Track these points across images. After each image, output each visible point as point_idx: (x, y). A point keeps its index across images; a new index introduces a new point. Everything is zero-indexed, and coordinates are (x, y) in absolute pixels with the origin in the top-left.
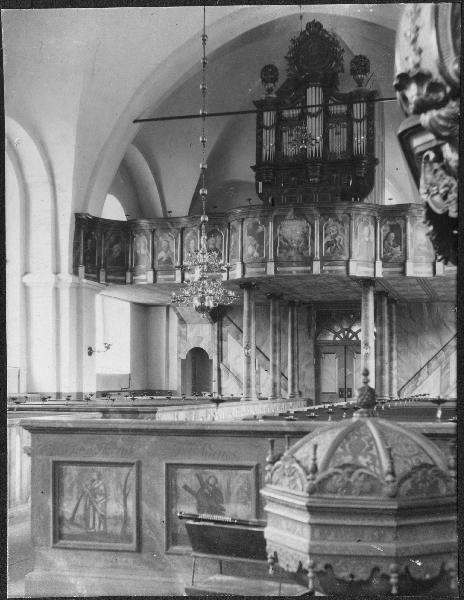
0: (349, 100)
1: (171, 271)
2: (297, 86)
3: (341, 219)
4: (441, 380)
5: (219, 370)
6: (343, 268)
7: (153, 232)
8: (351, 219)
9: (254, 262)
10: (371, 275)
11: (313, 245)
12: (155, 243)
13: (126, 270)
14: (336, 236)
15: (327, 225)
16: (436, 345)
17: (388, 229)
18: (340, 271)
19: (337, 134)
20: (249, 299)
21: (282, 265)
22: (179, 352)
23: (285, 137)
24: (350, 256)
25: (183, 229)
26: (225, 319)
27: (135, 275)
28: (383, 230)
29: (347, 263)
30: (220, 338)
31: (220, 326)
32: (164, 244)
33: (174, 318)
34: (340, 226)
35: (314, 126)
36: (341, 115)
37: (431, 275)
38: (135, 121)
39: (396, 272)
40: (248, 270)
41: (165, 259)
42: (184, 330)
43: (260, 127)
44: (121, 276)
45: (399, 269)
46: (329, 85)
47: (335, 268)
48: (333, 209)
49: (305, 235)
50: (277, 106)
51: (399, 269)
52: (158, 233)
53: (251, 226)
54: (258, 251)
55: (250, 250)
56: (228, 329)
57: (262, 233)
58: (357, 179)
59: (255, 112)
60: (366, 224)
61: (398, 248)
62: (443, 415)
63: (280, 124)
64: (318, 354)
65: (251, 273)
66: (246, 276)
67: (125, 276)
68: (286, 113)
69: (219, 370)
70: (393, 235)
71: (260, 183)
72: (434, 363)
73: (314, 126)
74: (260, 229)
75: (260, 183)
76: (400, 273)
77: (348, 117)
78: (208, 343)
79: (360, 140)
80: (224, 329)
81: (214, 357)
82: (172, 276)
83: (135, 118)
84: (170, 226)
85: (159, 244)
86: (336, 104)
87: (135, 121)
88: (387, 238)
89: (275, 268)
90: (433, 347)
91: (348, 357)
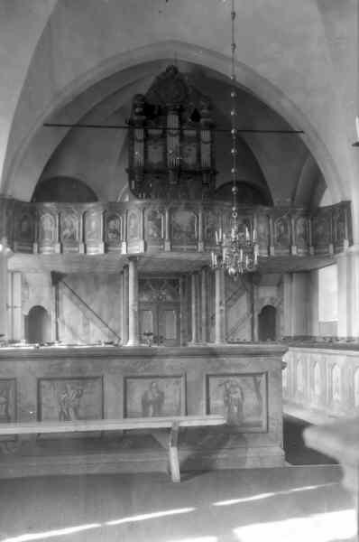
1: (76, 245)
5: (57, 323)
13: (33, 242)
18: (68, 247)
19: (155, 148)
21: (177, 244)
23: (151, 148)
25: (85, 213)
30: (57, 298)
31: (57, 289)
32: (69, 224)
33: (17, 278)
35: (173, 142)
38: (46, 125)
41: (69, 235)
42: (26, 292)
49: (192, 223)
50: (144, 125)
51: (110, 248)
57: (161, 220)
59: (125, 127)
63: (147, 138)
67: (32, 246)
68: (152, 132)
69: (57, 323)
73: (173, 142)
74: (158, 217)
75: (133, 182)
77: (198, 139)
78: (48, 303)
80: (60, 292)
81: (53, 314)
82: (76, 249)
86: (189, 129)
87: (46, 125)
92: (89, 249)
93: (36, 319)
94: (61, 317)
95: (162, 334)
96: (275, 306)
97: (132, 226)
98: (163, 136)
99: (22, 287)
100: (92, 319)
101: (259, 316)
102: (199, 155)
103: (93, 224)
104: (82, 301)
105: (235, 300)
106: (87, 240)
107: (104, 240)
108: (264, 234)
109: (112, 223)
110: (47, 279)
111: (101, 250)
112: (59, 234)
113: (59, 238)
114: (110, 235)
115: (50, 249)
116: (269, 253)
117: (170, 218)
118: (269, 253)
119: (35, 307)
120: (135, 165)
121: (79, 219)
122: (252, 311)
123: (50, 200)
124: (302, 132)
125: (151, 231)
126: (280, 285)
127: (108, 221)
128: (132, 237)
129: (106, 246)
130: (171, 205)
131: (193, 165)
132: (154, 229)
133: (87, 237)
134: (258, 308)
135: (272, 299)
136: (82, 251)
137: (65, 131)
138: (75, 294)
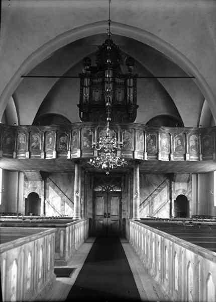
0: (126, 77)
1: (40, 153)
2: (102, 68)
3: (131, 131)
4: (150, 210)
5: (44, 204)
6: (131, 155)
8: (135, 132)
9: (87, 149)
10: (143, 159)
12: (30, 139)
13: (14, 151)
14: (128, 139)
15: (124, 133)
16: (147, 194)
17: (150, 138)
20: (78, 169)
22: (24, 194)
24: (135, 149)
26: (48, 179)
27: (18, 154)
28: (148, 137)
29: (133, 152)
30: (45, 188)
32: (35, 139)
33: (22, 175)
34: (130, 135)
36: (121, 84)
37: (168, 160)
38: (22, 77)
39: (154, 158)
41: (35, 147)
43: (82, 85)
44: (91, 152)
45: (155, 157)
46: (115, 68)
47: (127, 154)
52: (32, 133)
53: (85, 132)
57: (91, 136)
60: (141, 134)
61: (154, 147)
63: (92, 85)
64: (95, 196)
65: (85, 155)
66: (83, 157)
67: (12, 154)
68: (95, 81)
69: (44, 204)
70: (152, 140)
71: (82, 113)
72: (146, 202)
74: (90, 133)
75: (82, 113)
77: (125, 85)
78: (40, 191)
79: (130, 96)
80: (47, 184)
81: (42, 197)
83: (22, 75)
84: (39, 130)
85: (33, 139)
87: (22, 77)
88: (149, 142)
89: (98, 153)
91: (109, 199)
93: (33, 200)
94: (47, 199)
95: (109, 212)
96: (186, 195)
98: (103, 83)
99: (24, 180)
100: (67, 202)
102: (126, 95)
105: (159, 191)
106: (47, 149)
108: (166, 146)
109: (62, 138)
110: (37, 175)
111: (54, 156)
112: (29, 146)
113: (29, 148)
114: (61, 147)
119: (29, 195)
121: (42, 136)
122: (171, 198)
123: (48, 125)
124: (194, 77)
125: (85, 143)
126: (189, 181)
127: (60, 137)
128: (74, 147)
129: (58, 153)
130: (99, 126)
132: (87, 142)
133: (46, 148)
134: (174, 196)
135: (184, 191)
136: (43, 157)
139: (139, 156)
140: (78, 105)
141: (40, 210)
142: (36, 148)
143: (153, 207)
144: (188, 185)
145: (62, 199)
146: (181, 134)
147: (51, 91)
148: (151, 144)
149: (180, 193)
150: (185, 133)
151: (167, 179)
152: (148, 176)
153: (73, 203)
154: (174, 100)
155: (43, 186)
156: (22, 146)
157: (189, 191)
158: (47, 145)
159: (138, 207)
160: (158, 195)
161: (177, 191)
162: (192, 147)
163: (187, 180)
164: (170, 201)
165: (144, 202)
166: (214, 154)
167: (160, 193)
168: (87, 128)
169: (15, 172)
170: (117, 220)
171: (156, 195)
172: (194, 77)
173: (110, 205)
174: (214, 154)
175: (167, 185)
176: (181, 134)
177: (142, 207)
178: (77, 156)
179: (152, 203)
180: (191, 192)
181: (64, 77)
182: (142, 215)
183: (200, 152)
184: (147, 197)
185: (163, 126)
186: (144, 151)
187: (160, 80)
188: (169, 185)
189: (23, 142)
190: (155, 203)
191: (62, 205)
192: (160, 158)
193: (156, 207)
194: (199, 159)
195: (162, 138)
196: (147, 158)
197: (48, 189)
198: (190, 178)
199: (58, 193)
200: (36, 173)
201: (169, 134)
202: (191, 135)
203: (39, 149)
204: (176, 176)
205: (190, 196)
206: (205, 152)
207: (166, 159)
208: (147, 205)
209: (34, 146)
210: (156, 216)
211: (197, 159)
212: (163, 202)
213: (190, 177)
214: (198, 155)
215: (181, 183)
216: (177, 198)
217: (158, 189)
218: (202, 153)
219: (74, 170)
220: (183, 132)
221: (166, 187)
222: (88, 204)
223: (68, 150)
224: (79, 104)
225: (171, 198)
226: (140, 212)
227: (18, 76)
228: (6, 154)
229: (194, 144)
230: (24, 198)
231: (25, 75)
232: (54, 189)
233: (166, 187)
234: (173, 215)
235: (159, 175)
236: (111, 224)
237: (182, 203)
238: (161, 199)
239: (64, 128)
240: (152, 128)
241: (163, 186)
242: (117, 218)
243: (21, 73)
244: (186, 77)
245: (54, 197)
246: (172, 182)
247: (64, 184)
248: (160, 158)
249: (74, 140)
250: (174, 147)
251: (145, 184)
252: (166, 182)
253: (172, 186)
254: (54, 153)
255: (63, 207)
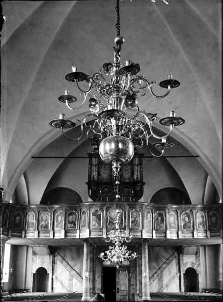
1: (48, 232)
5: (52, 279)
6: (140, 234)
7: (39, 212)
10: (151, 237)
11: (125, 222)
13: (23, 230)
14: (136, 218)
18: (43, 233)
20: (87, 247)
23: (102, 170)
26: (56, 253)
29: (142, 231)
30: (54, 262)
32: (44, 218)
33: (30, 250)
38: (33, 157)
40: (92, 233)
41: (44, 226)
43: (90, 164)
48: (135, 205)
54: (98, 224)
55: (93, 223)
56: (58, 259)
57: (100, 215)
58: (136, 191)
60: (149, 213)
62: (101, 296)
66: (91, 236)
67: (21, 233)
69: (52, 279)
70: (159, 218)
71: (90, 191)
72: (155, 276)
74: (99, 213)
75: (90, 191)
76: (68, 232)
78: (47, 264)
79: (137, 174)
80: (56, 258)
81: (50, 272)
82: (49, 234)
87: (33, 157)
88: (157, 219)
90: (154, 268)
92: (56, 234)
93: (41, 276)
94: (55, 274)
96: (195, 268)
97: (83, 220)
100: (75, 277)
101: (184, 274)
102: (99, 174)
103: (60, 218)
104: (69, 264)
105: (168, 264)
107: (65, 228)
109: (71, 217)
110: (45, 250)
111: (63, 236)
114: (69, 226)
115: (32, 234)
116: (178, 236)
117: (106, 215)
118: (178, 236)
119: (39, 268)
120: (92, 179)
122: (180, 271)
123: (56, 204)
124: (198, 156)
125: (94, 223)
126: (197, 254)
127: (69, 216)
129: (66, 232)
131: (129, 179)
132: (96, 221)
133: (55, 227)
135: (192, 263)
136: (51, 237)
137: (62, 160)
138: (64, 259)
139: (95, 233)
140: (87, 183)
141: (47, 284)
142: (45, 227)
143: (162, 281)
144: (196, 258)
145: (70, 274)
146: (188, 211)
147: (60, 167)
148: (159, 222)
149: (189, 266)
150: (191, 211)
151: (175, 251)
152: (157, 249)
153: (82, 278)
154: (179, 174)
155: (52, 260)
156: (31, 226)
157: (198, 263)
158: (56, 224)
159: (148, 286)
160: (167, 268)
161: (186, 264)
162: (200, 224)
163: (195, 252)
164: (178, 275)
165: (153, 276)
166: (221, 231)
167: (169, 266)
168: (96, 207)
169: (23, 247)
170: (126, 296)
171: (165, 268)
172: (198, 156)
173: (119, 279)
174: (221, 231)
175: (176, 257)
176: (188, 211)
177: (152, 281)
178: (85, 235)
179: (161, 277)
180: (199, 264)
181: (71, 157)
182: (152, 289)
183: (208, 229)
184: (155, 271)
185: (171, 203)
186: (152, 229)
187: (167, 158)
188: (177, 258)
189: (32, 221)
190: (164, 277)
191: (70, 280)
192: (168, 237)
193: (165, 282)
194: (207, 236)
195: (169, 217)
196: (156, 236)
197: (56, 263)
198: (198, 250)
199: (66, 268)
200: (44, 248)
201: (176, 211)
202: (197, 212)
203: (47, 228)
204: (184, 249)
205: (199, 268)
206: (213, 228)
207: (174, 236)
208: (155, 279)
209: (42, 226)
210: (165, 291)
211: (205, 236)
212: (172, 275)
213: (198, 249)
214: (206, 231)
215: (189, 256)
216: (186, 272)
217: (167, 261)
218: (209, 229)
219: (83, 246)
220: (190, 209)
221: (175, 260)
222: (96, 279)
223: (77, 229)
224: (87, 181)
225: (180, 271)
226: (150, 285)
227: (28, 158)
228: (15, 234)
229: (201, 221)
230: (32, 273)
231: (36, 156)
232: (62, 263)
233: (175, 260)
234: (183, 290)
235: (167, 248)
236: (121, 300)
237: (191, 276)
238: (170, 272)
239: (73, 204)
240: (160, 201)
241: (172, 259)
242: (126, 293)
243: (30, 155)
244: (191, 157)
245: (62, 272)
246: (181, 255)
247: (73, 259)
248: (168, 237)
249: (83, 220)
250: (182, 224)
251: (154, 258)
252: (174, 255)
253: (181, 259)
254: (63, 231)
255: (71, 282)
